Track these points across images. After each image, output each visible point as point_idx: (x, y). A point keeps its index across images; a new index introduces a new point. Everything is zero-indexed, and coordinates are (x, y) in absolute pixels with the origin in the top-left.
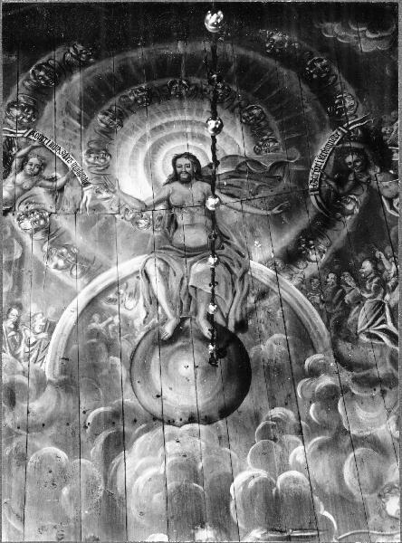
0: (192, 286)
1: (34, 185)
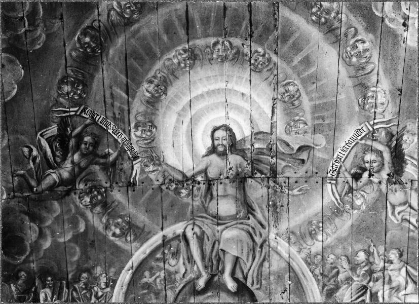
0: (221, 250)
1: (91, 163)
